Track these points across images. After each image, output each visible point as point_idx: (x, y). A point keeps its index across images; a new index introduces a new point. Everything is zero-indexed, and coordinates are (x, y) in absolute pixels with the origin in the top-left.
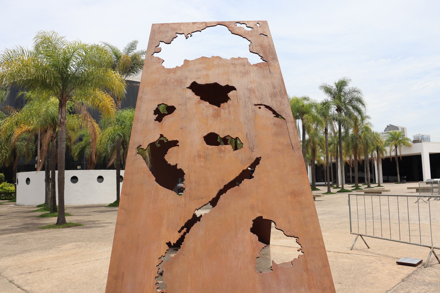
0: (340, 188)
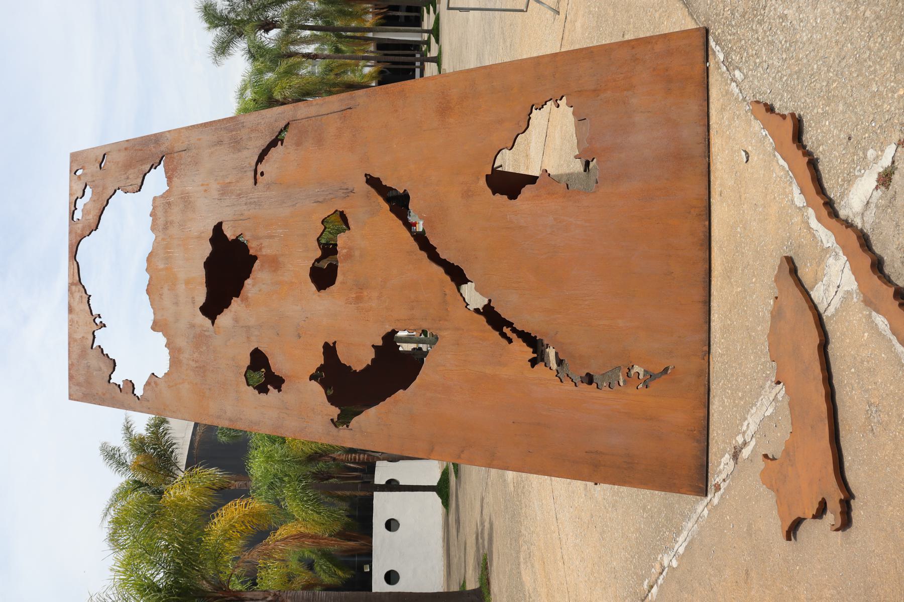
0: (429, 38)
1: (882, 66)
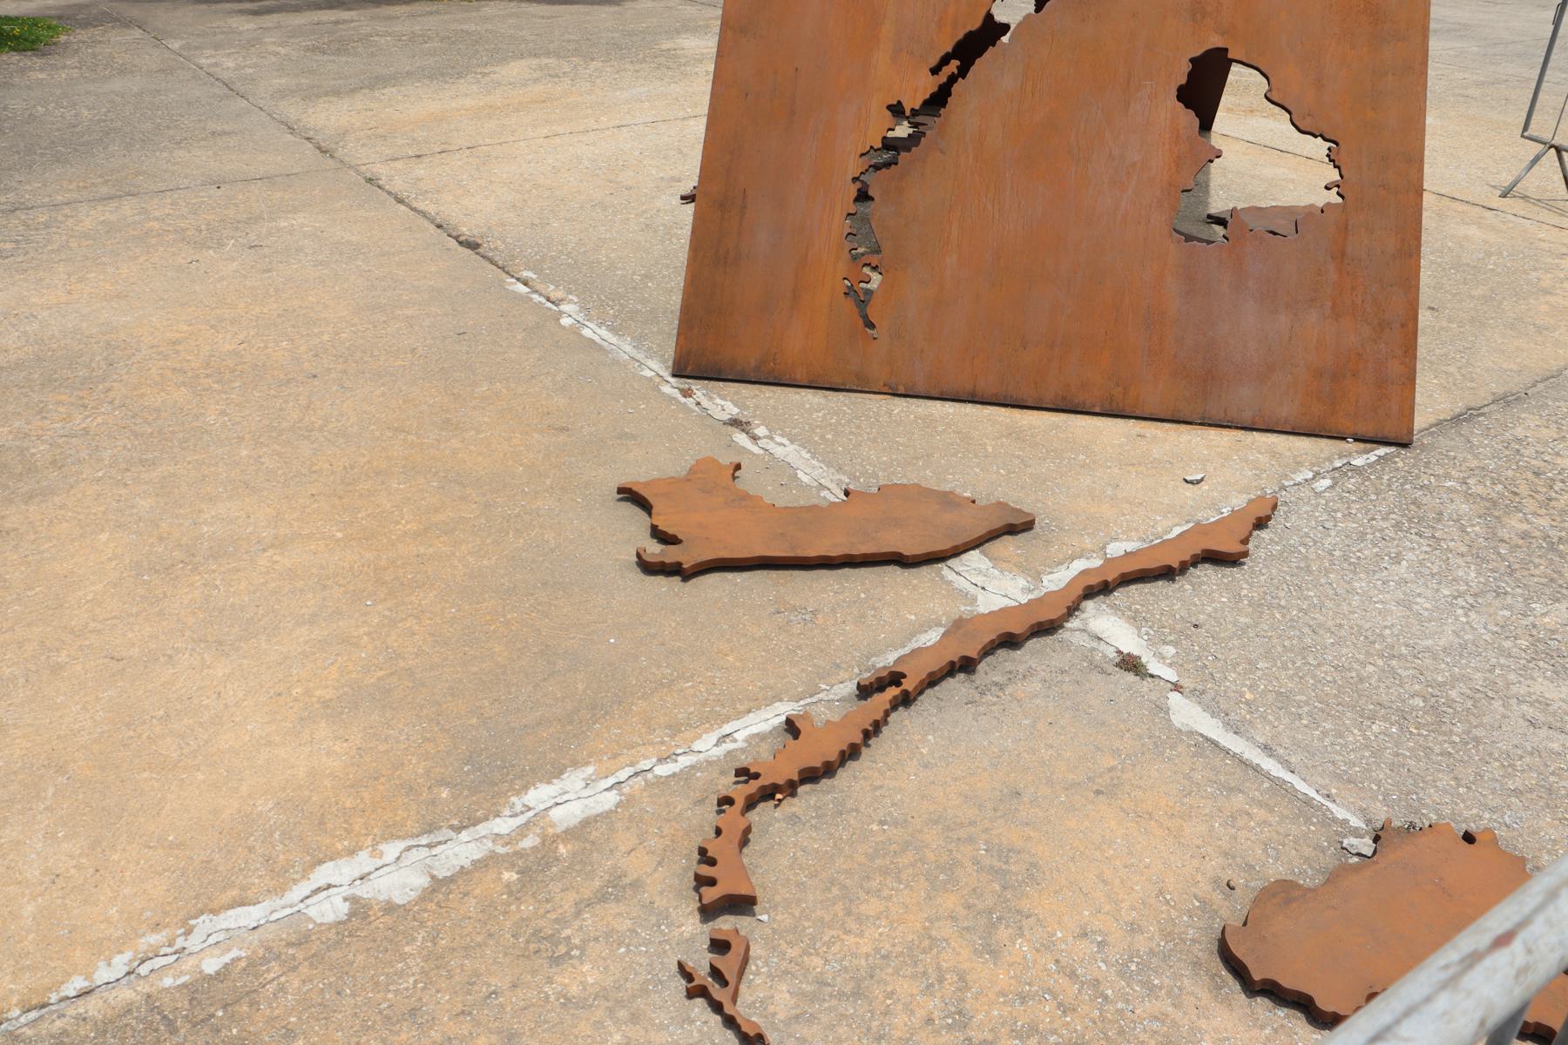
1: (1291, 678)
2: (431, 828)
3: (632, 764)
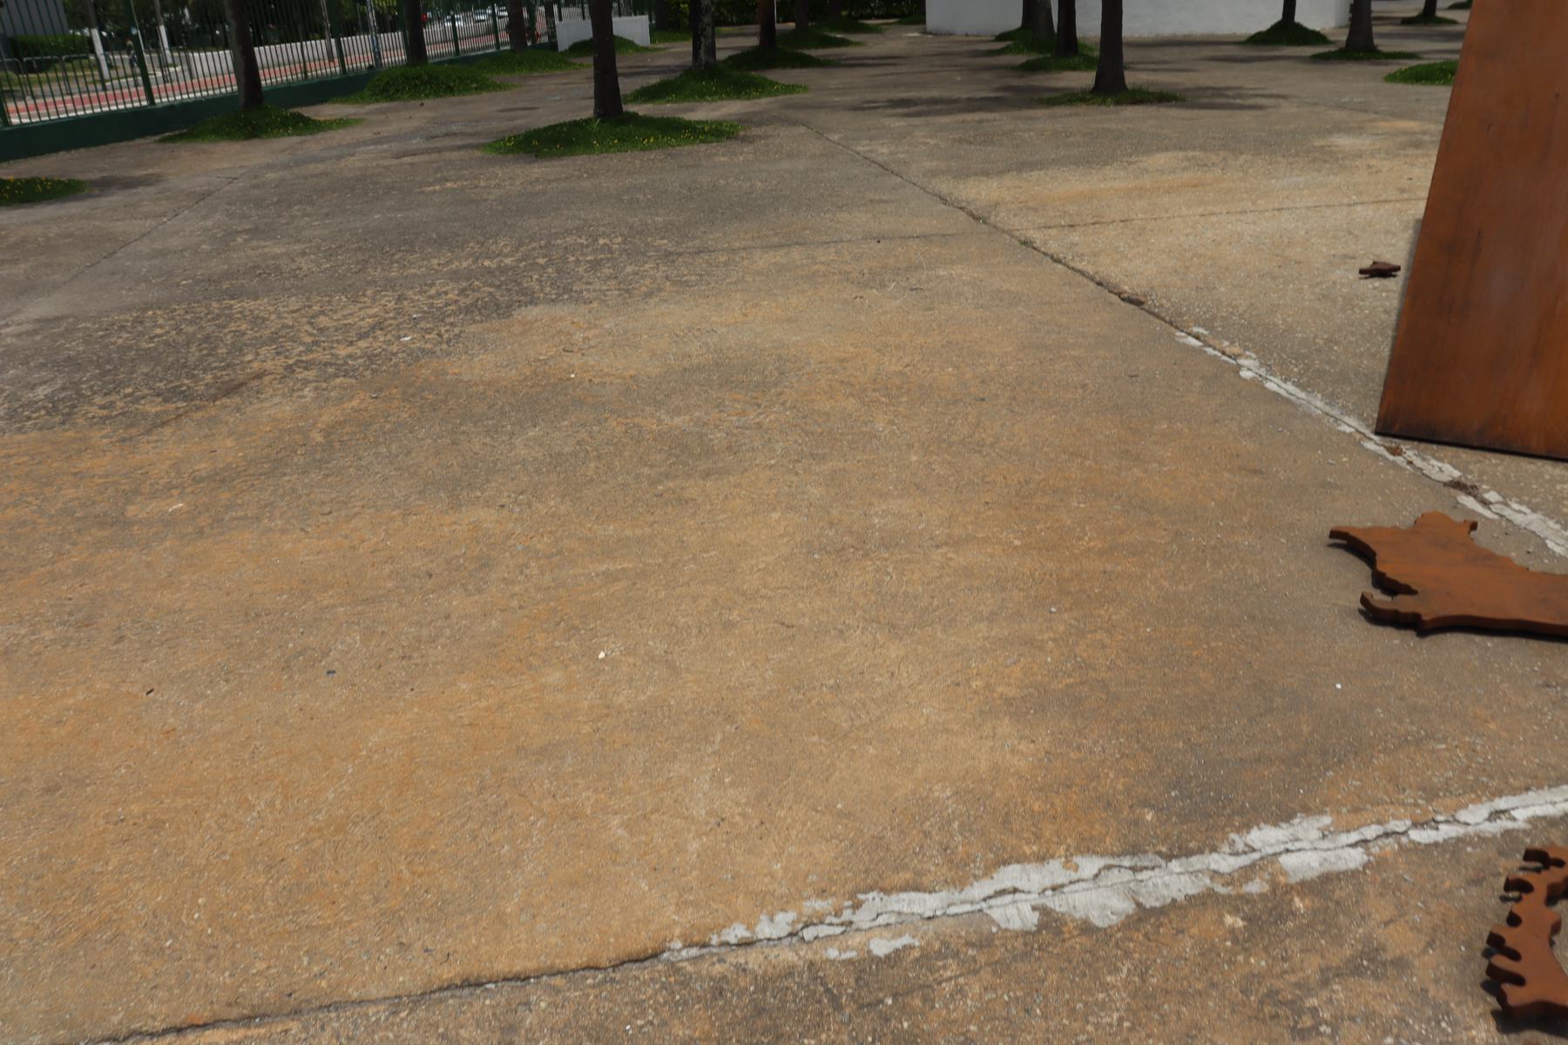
2: (1134, 850)
3: (1379, 822)
